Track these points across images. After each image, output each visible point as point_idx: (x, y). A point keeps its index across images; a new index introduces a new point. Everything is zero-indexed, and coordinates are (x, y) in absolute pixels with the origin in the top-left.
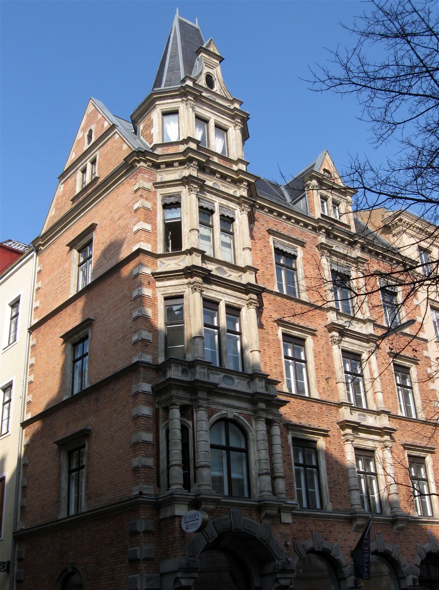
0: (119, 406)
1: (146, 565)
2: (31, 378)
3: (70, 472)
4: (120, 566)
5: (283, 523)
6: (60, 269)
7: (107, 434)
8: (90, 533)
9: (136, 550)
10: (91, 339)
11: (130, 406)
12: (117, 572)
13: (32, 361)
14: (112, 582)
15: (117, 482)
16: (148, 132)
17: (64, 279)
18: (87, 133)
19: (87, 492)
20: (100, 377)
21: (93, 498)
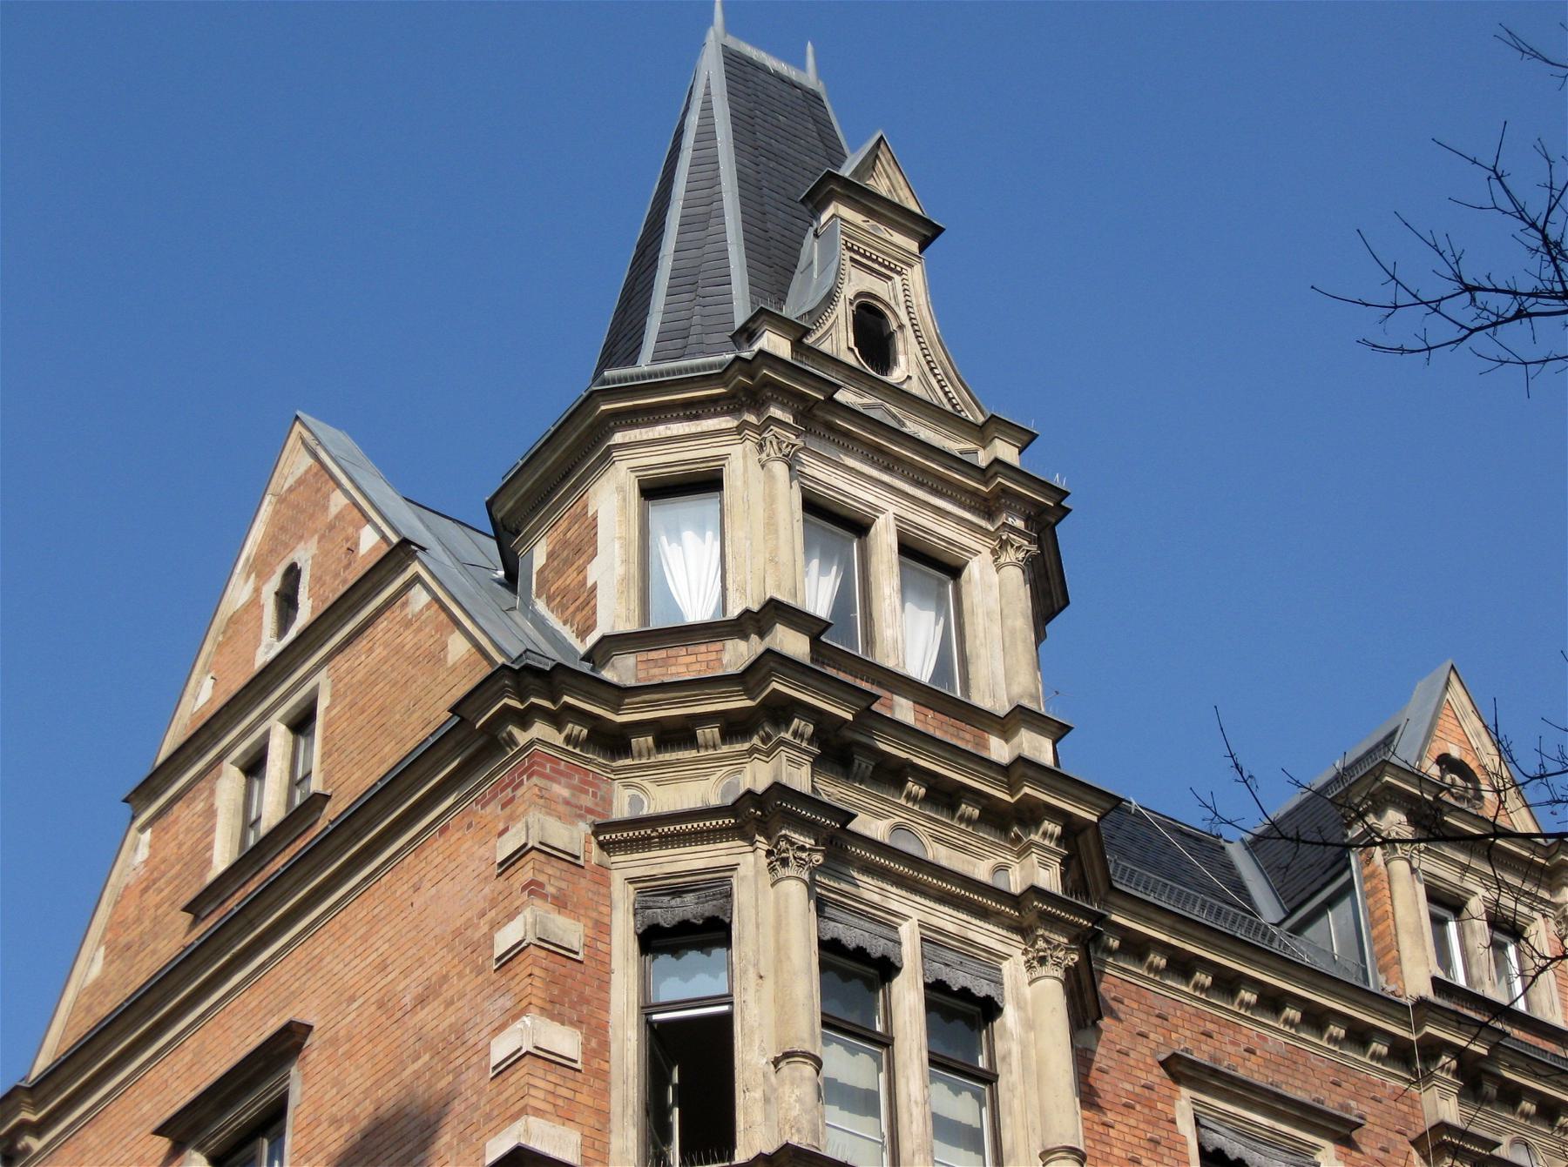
16: (570, 577)
18: (274, 583)
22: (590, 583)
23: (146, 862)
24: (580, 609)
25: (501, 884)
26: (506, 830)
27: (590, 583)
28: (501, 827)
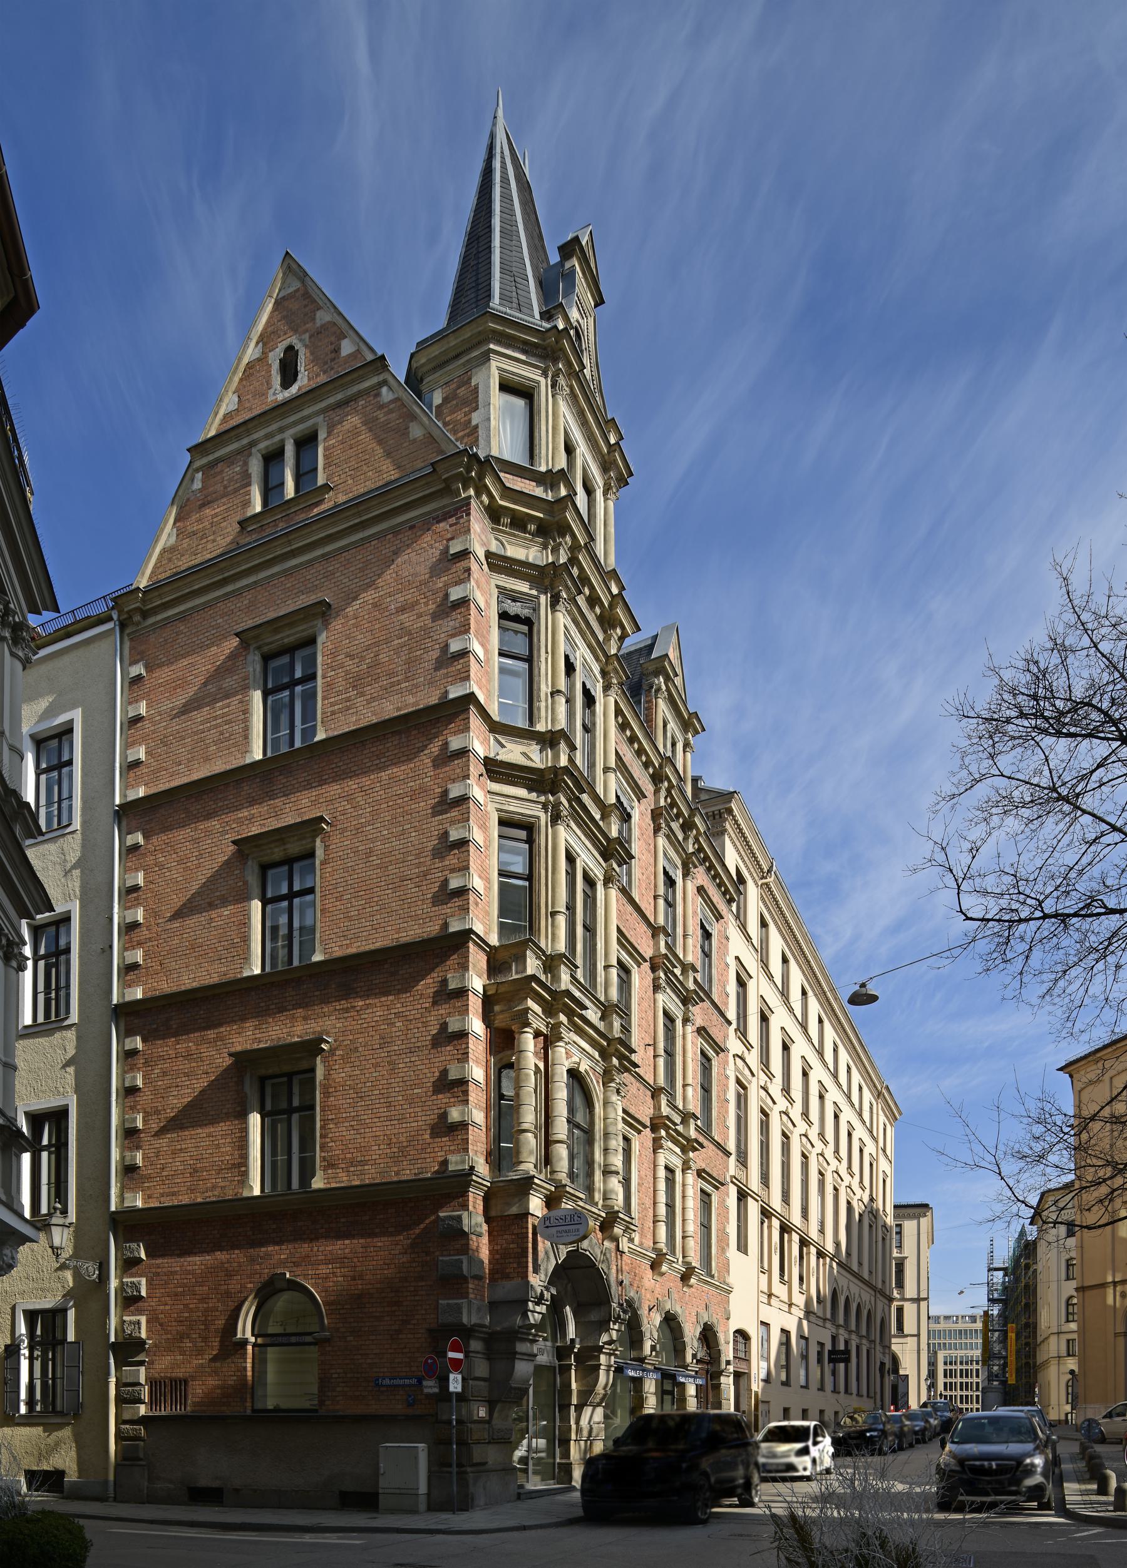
22: (474, 423)
23: (200, 490)
27: (474, 423)
28: (449, 536)
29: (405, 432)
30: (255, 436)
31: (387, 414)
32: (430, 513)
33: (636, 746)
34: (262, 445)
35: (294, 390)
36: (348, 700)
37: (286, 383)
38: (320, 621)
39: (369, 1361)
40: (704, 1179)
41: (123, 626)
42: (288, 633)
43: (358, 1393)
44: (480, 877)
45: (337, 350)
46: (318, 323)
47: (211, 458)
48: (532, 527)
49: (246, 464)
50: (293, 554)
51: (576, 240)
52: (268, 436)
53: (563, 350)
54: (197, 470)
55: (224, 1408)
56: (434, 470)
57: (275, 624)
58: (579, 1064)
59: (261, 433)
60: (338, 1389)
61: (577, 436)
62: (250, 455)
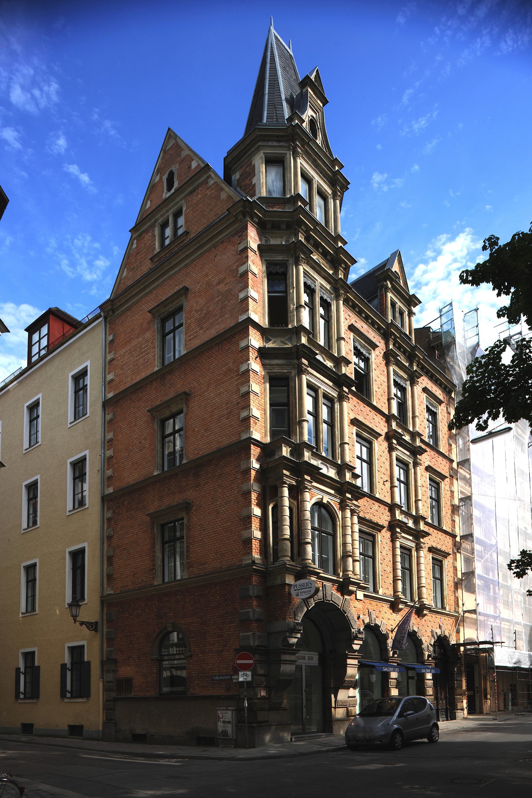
0: (225, 481)
1: (256, 625)
2: (109, 453)
3: (163, 543)
4: (228, 625)
5: (357, 600)
6: (140, 339)
7: (210, 508)
8: (192, 597)
9: (249, 612)
10: (186, 414)
11: (239, 481)
12: (225, 631)
13: (110, 436)
14: (220, 639)
15: (224, 552)
16: (247, 182)
17: (146, 350)
18: (165, 178)
19: (188, 561)
20: (201, 453)
21: (196, 566)
22: (253, 183)
23: (136, 248)
24: (250, 190)
25: (239, 257)
26: (240, 243)
27: (253, 183)
28: (239, 242)
29: (218, 197)
30: (156, 217)
31: (210, 191)
32: (229, 233)
33: (370, 321)
34: (160, 221)
35: (173, 191)
36: (196, 332)
37: (169, 189)
38: (184, 297)
39: (209, 667)
40: (433, 552)
41: (106, 318)
42: (171, 306)
43: (204, 684)
44: (258, 409)
45: (190, 167)
46: (182, 156)
47: (139, 232)
48: (283, 226)
49: (154, 231)
50: (173, 268)
51: (307, 78)
52: (162, 216)
53: (297, 134)
54: (134, 239)
55: (147, 693)
56: (229, 212)
57: (164, 304)
58: (322, 499)
59: (159, 215)
60: (196, 682)
61: (312, 173)
62: (155, 226)
